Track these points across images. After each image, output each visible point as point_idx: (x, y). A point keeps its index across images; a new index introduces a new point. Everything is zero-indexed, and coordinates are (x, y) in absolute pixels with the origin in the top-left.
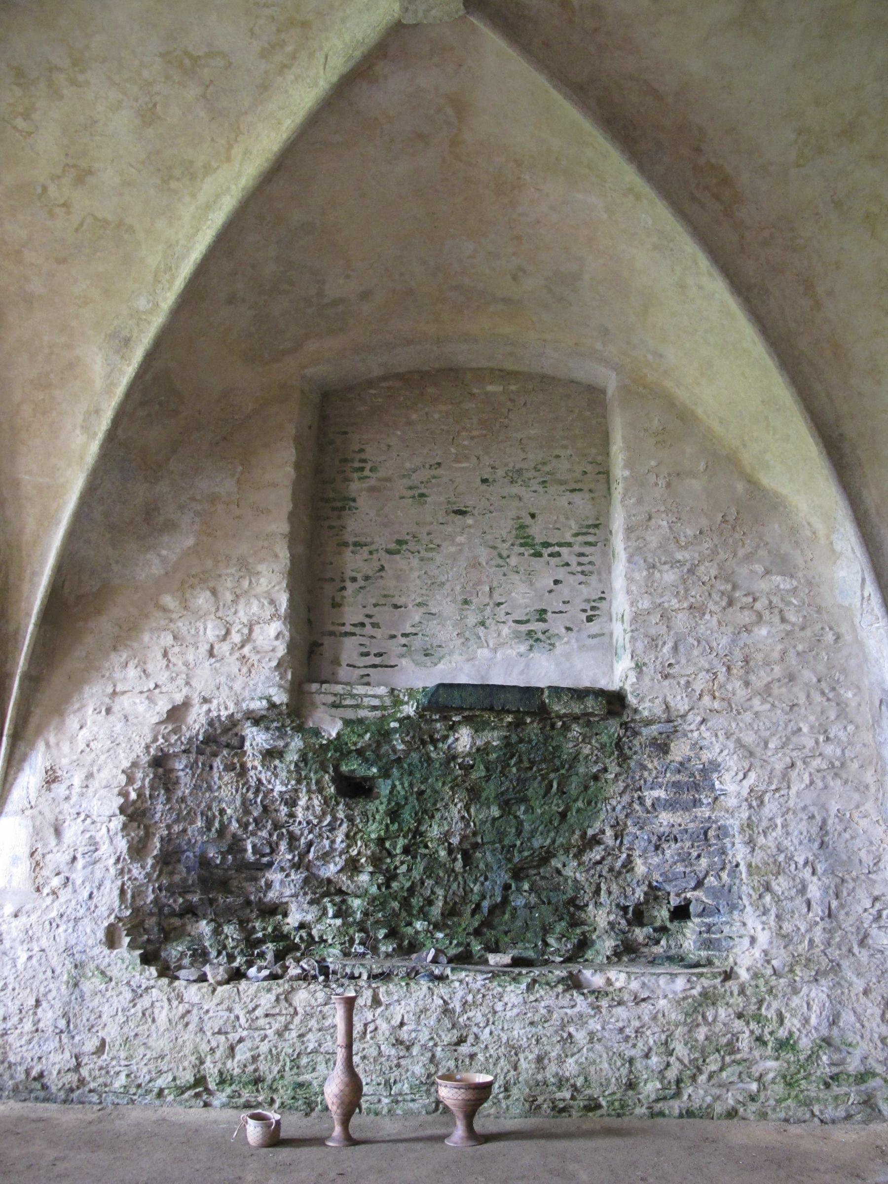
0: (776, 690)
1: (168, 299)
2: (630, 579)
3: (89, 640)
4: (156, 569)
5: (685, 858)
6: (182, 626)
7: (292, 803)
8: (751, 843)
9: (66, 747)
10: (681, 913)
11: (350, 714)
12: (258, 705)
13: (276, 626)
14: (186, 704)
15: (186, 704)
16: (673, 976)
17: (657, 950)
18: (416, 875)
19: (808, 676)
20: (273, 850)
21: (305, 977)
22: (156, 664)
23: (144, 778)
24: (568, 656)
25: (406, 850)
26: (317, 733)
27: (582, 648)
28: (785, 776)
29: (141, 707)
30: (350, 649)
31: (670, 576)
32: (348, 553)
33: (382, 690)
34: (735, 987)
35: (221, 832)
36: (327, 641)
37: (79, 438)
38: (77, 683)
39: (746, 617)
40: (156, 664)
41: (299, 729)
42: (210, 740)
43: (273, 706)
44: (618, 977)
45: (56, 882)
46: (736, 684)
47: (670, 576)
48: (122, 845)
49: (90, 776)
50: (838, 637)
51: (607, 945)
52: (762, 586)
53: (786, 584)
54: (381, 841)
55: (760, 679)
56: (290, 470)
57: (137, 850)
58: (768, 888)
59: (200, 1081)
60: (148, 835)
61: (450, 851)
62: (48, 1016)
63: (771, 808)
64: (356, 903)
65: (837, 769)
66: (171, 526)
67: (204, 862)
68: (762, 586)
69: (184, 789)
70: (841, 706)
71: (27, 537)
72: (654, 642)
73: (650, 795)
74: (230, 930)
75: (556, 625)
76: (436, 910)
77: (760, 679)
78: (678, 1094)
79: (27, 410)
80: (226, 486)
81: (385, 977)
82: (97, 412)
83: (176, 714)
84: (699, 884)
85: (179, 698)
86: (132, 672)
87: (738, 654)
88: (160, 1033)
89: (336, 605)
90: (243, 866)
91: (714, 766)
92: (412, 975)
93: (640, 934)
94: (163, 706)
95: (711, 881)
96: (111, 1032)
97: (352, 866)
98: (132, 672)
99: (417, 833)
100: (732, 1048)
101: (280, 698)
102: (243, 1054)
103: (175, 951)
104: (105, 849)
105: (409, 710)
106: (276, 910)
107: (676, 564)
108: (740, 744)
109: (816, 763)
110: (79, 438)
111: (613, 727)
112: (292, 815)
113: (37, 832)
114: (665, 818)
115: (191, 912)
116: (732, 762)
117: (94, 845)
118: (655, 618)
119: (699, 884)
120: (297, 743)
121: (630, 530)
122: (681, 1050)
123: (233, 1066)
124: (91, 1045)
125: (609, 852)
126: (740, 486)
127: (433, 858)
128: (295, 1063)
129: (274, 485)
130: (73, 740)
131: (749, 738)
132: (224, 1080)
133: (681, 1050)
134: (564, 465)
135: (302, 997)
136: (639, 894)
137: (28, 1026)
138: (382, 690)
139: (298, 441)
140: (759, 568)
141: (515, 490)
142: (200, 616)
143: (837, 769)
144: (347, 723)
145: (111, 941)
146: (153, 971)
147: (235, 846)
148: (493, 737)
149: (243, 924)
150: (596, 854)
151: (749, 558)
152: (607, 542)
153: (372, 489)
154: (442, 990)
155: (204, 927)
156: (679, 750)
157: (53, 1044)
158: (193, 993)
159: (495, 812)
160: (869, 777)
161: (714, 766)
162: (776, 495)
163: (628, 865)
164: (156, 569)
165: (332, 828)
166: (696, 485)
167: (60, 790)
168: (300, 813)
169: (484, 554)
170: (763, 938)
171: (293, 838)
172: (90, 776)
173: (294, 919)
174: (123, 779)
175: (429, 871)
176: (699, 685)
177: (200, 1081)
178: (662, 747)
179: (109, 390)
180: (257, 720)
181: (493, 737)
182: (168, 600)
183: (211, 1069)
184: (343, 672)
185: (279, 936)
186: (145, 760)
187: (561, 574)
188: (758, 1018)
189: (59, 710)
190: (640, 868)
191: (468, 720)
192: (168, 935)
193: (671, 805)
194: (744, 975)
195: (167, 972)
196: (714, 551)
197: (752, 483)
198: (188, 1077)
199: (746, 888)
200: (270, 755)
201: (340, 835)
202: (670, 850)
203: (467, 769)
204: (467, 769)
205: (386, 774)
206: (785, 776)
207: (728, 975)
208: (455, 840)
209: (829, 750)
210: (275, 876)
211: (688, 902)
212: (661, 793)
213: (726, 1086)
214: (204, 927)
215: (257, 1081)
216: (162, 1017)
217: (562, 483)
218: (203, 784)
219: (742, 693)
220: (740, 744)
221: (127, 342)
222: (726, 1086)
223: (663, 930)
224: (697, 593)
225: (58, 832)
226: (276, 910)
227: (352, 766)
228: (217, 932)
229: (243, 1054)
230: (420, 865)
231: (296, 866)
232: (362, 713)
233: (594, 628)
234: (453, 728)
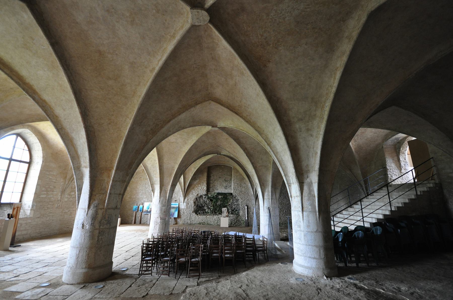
0: (244, 194)
1: (199, 166)
2: (233, 185)
3: (190, 188)
4: (196, 183)
5: (237, 206)
6: (198, 188)
7: (206, 201)
8: (241, 205)
9: (189, 197)
10: (236, 210)
11: (211, 195)
12: (204, 194)
13: (205, 188)
14: (198, 194)
15: (198, 194)
16: (235, 215)
17: (234, 213)
18: (216, 207)
19: (246, 193)
20: (205, 205)
21: (208, 215)
22: (196, 191)
23: (195, 200)
24: (228, 190)
25: (215, 205)
26: (209, 196)
27: (230, 189)
28: (244, 200)
29: (195, 194)
30: (211, 189)
31: (236, 184)
32: (211, 181)
33: (214, 193)
34: (239, 216)
35: (201, 204)
36: (209, 188)
37: (191, 174)
38: (189, 192)
39: (242, 188)
40: (196, 191)
41: (207, 196)
42: (200, 196)
43: (205, 194)
44: (231, 215)
45: (188, 208)
46: (241, 193)
47: (236, 184)
48: (194, 205)
49: (191, 200)
50: (249, 189)
51: (230, 213)
52: (243, 185)
53: (245, 185)
54: (213, 205)
55: (243, 193)
56: (206, 175)
57: (195, 205)
58: (242, 209)
59: (200, 223)
60: (196, 204)
61: (219, 205)
62: (188, 218)
63: (243, 203)
64: (212, 209)
65: (248, 200)
66: (197, 179)
67: (200, 206)
68: (243, 185)
69: (198, 200)
70: (249, 195)
71: (186, 181)
72: (235, 190)
73: (234, 201)
74: (202, 212)
75: (227, 187)
76: (218, 210)
77: (243, 193)
78: (235, 224)
79: (187, 172)
80: (201, 176)
81: (214, 215)
82: (193, 173)
83: (198, 195)
84: (237, 208)
85: (198, 193)
86: (194, 191)
87: (241, 191)
88: (68, 297)
89: (210, 185)
90: (203, 206)
91: (239, 199)
92: (216, 215)
93: (233, 212)
94: (197, 194)
95: (238, 208)
96: (193, 219)
97: (211, 206)
98: (194, 191)
99: (216, 204)
100: (239, 221)
101: (206, 193)
102: (203, 221)
103: (198, 213)
104: (192, 205)
105: (216, 194)
106: (205, 210)
107: (237, 183)
108: (241, 198)
109: (247, 199)
110: (191, 174)
111: (231, 196)
112: (206, 202)
113: (187, 204)
114: (235, 203)
115: (199, 210)
116: (240, 199)
117: (191, 205)
118: (235, 188)
119: (237, 208)
120: (207, 197)
121: (233, 180)
122: (235, 221)
123: (203, 222)
124: (192, 220)
125: (231, 206)
126: (242, 177)
127: (217, 206)
128: (207, 221)
129: (205, 176)
130: (189, 197)
131: (242, 197)
132: (202, 223)
133: (235, 221)
134: (228, 174)
135: (208, 216)
136: (233, 209)
137: (187, 219)
138: (214, 193)
139: (207, 172)
140: (243, 184)
141: (224, 176)
142: (199, 187)
143: (248, 200)
144: (211, 195)
145: (193, 212)
146: (196, 215)
147: (202, 205)
148: (222, 197)
149: (203, 211)
150: (230, 206)
151: (242, 183)
152: (232, 180)
153: (213, 175)
154: (218, 216)
155: (200, 211)
156: (236, 198)
157: (189, 220)
158: (199, 216)
159: (222, 202)
160: (251, 201)
161: (239, 199)
162: (245, 178)
163: (232, 207)
164: (196, 183)
165: (210, 203)
166: (239, 177)
167: (189, 201)
168: (207, 202)
169: (222, 181)
170: (242, 213)
171: (207, 204)
172: (191, 200)
173: (206, 211)
174: (194, 200)
175: (217, 207)
176: (238, 193)
177: (200, 223)
178: (235, 198)
179: (194, 171)
180: (204, 195)
181: (222, 197)
182: (197, 185)
183: (201, 222)
184: (210, 191)
185: (205, 212)
186: (195, 198)
187: (228, 183)
188: (241, 218)
189: (188, 195)
190: (233, 207)
191: (220, 195)
192: (197, 212)
193: (236, 202)
194: (240, 215)
195: (197, 215)
196: (240, 182)
197: (243, 177)
198: (199, 223)
199: (241, 209)
200: (205, 198)
201: (210, 204)
202: (235, 205)
203: (220, 199)
204: (220, 199)
205: (214, 199)
206: (244, 200)
207: (239, 215)
208: (219, 204)
209: (248, 198)
210: (205, 207)
211: (237, 210)
212: (235, 201)
213: (239, 223)
214: (200, 211)
215: (204, 223)
216: (197, 218)
217: (228, 175)
218: (200, 200)
219: (241, 194)
220: (241, 198)
221: (195, 168)
222: (239, 223)
223: (235, 212)
224: (238, 186)
225: (188, 204)
226: (205, 210)
227: (211, 199)
228: (201, 212)
229: (203, 221)
230: (216, 206)
231: (207, 206)
232: (212, 194)
233: (230, 188)
234: (219, 196)
